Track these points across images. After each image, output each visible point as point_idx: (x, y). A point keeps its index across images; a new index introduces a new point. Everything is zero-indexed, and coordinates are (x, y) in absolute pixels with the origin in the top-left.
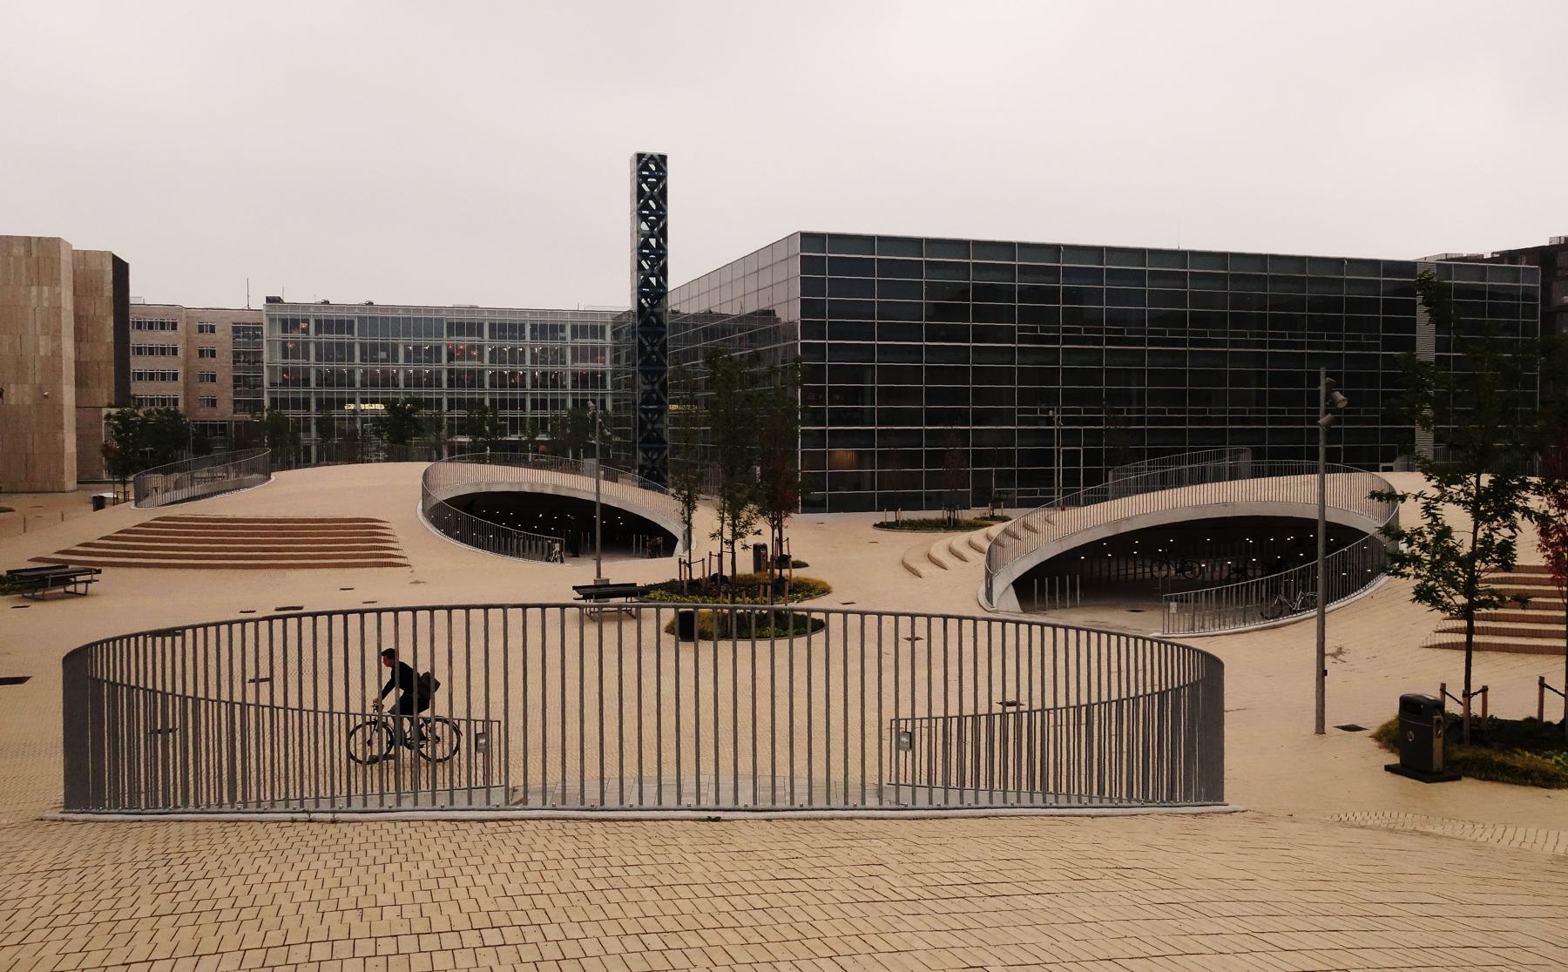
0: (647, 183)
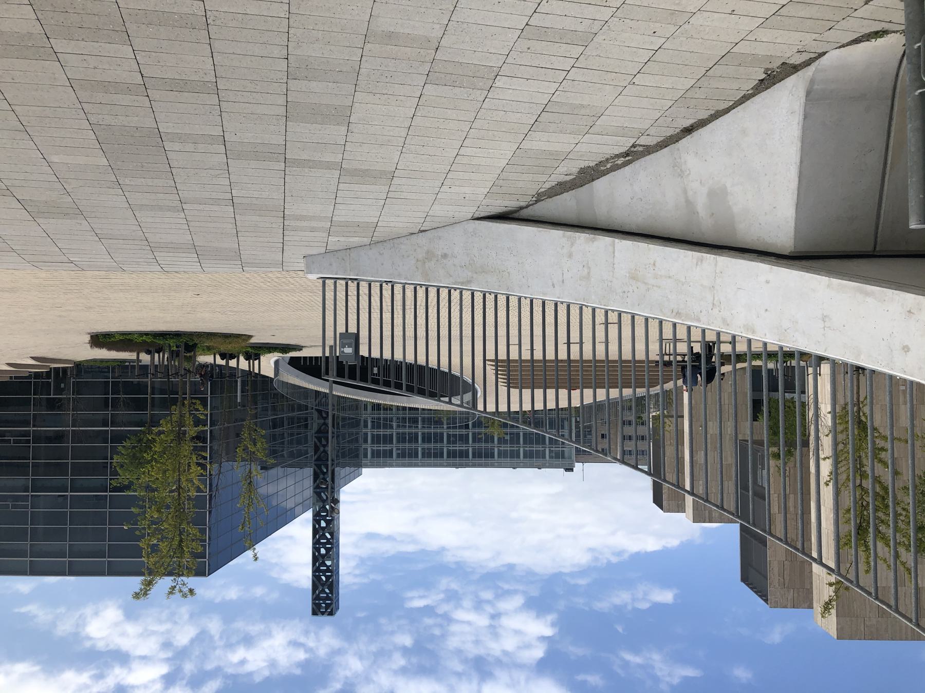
0: (326, 538)
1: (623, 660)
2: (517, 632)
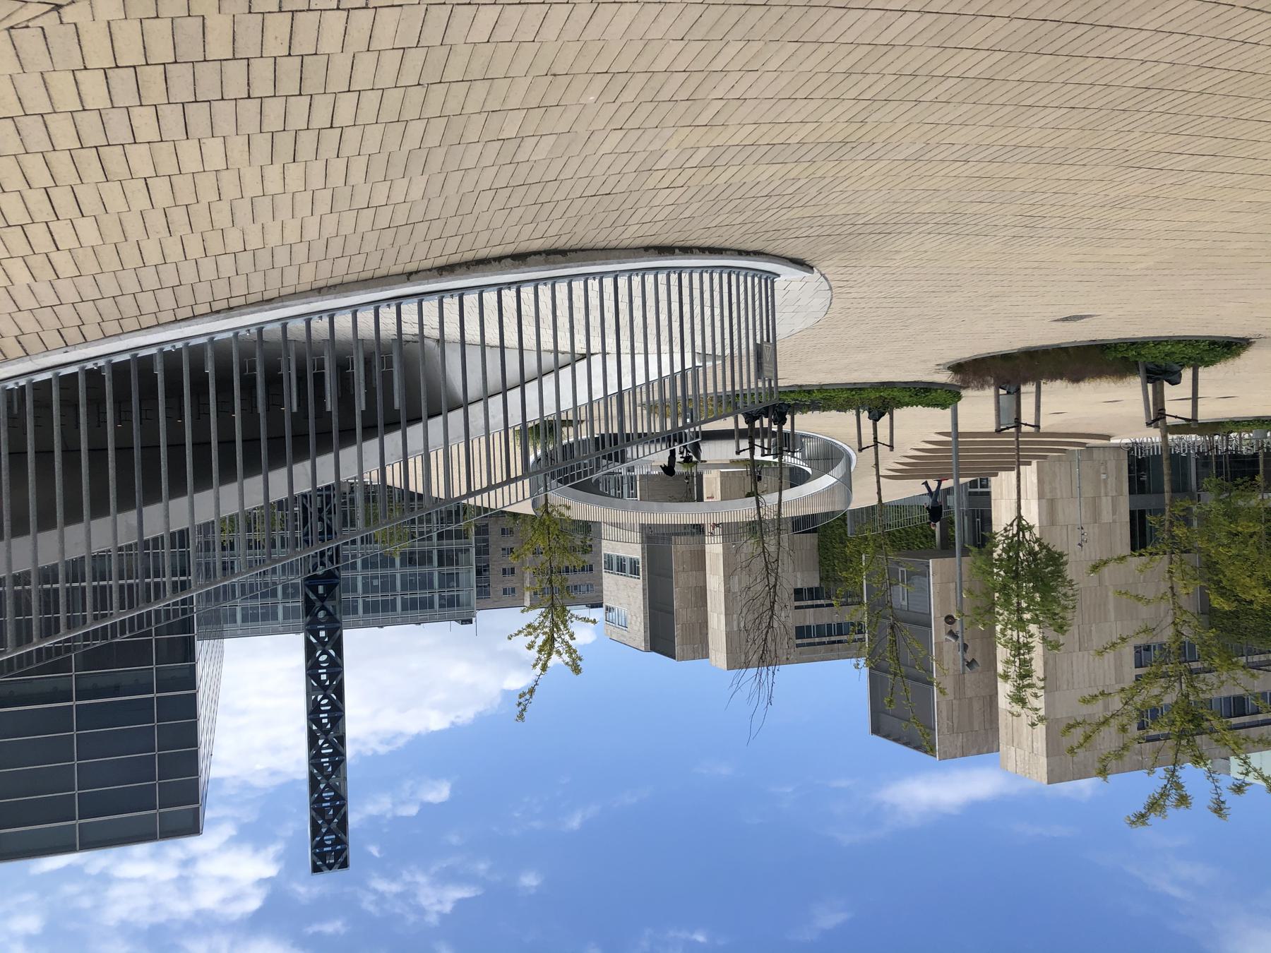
1: (375, 891)
2: (223, 880)
